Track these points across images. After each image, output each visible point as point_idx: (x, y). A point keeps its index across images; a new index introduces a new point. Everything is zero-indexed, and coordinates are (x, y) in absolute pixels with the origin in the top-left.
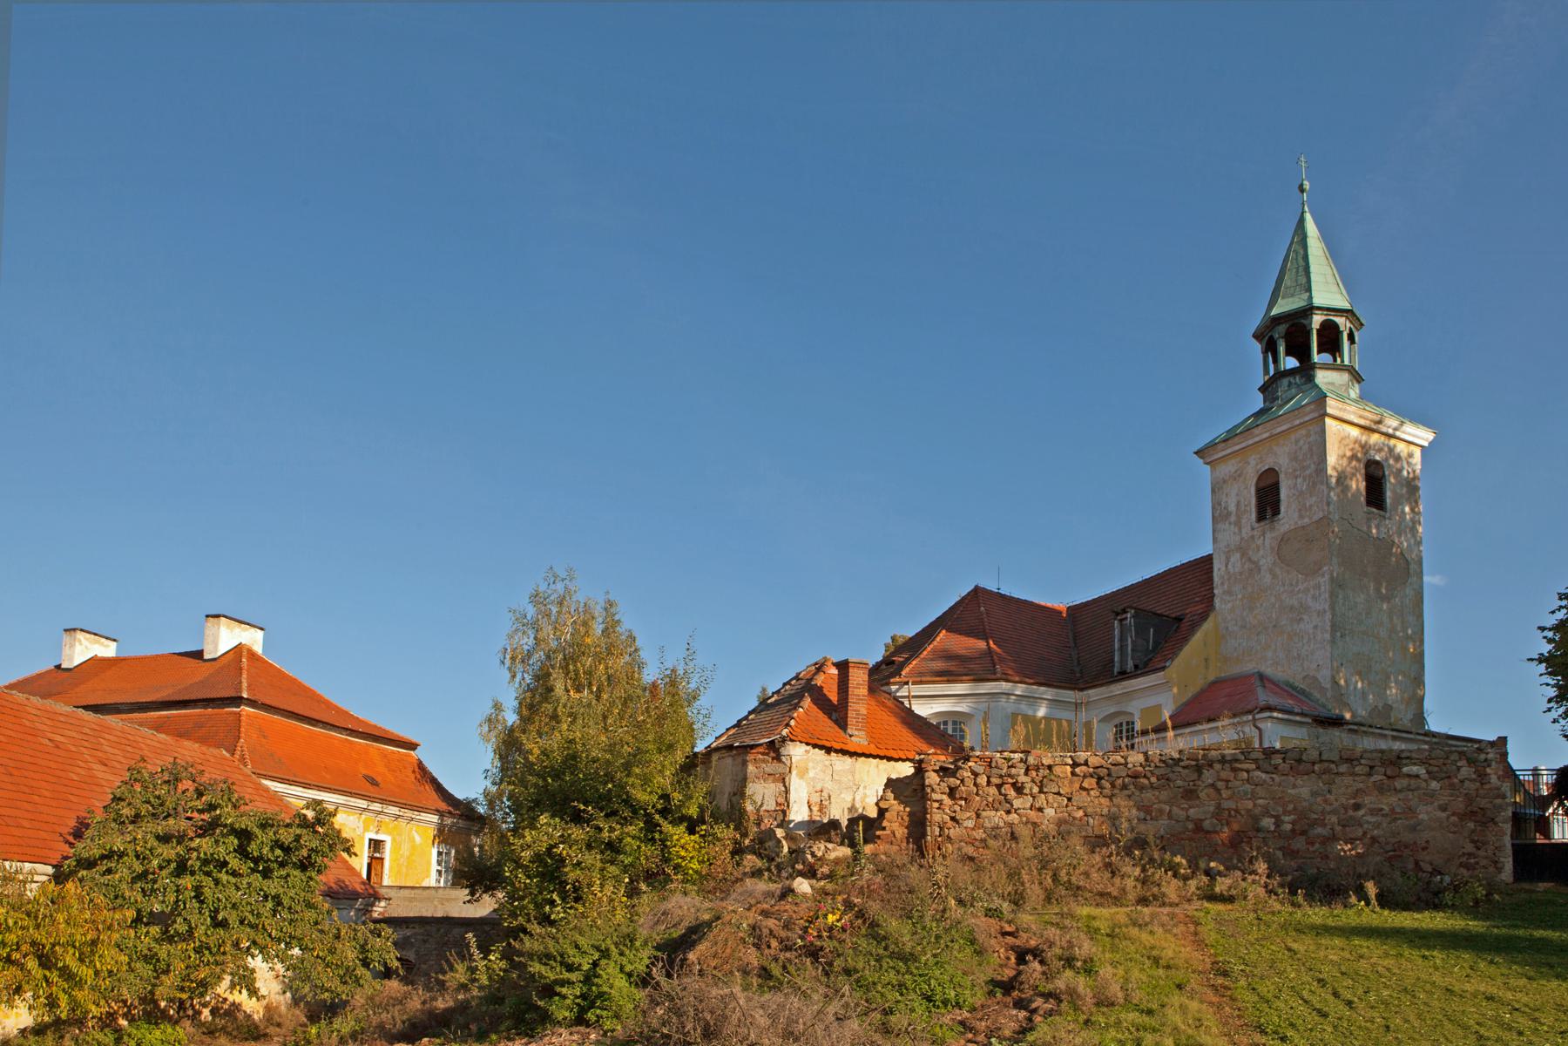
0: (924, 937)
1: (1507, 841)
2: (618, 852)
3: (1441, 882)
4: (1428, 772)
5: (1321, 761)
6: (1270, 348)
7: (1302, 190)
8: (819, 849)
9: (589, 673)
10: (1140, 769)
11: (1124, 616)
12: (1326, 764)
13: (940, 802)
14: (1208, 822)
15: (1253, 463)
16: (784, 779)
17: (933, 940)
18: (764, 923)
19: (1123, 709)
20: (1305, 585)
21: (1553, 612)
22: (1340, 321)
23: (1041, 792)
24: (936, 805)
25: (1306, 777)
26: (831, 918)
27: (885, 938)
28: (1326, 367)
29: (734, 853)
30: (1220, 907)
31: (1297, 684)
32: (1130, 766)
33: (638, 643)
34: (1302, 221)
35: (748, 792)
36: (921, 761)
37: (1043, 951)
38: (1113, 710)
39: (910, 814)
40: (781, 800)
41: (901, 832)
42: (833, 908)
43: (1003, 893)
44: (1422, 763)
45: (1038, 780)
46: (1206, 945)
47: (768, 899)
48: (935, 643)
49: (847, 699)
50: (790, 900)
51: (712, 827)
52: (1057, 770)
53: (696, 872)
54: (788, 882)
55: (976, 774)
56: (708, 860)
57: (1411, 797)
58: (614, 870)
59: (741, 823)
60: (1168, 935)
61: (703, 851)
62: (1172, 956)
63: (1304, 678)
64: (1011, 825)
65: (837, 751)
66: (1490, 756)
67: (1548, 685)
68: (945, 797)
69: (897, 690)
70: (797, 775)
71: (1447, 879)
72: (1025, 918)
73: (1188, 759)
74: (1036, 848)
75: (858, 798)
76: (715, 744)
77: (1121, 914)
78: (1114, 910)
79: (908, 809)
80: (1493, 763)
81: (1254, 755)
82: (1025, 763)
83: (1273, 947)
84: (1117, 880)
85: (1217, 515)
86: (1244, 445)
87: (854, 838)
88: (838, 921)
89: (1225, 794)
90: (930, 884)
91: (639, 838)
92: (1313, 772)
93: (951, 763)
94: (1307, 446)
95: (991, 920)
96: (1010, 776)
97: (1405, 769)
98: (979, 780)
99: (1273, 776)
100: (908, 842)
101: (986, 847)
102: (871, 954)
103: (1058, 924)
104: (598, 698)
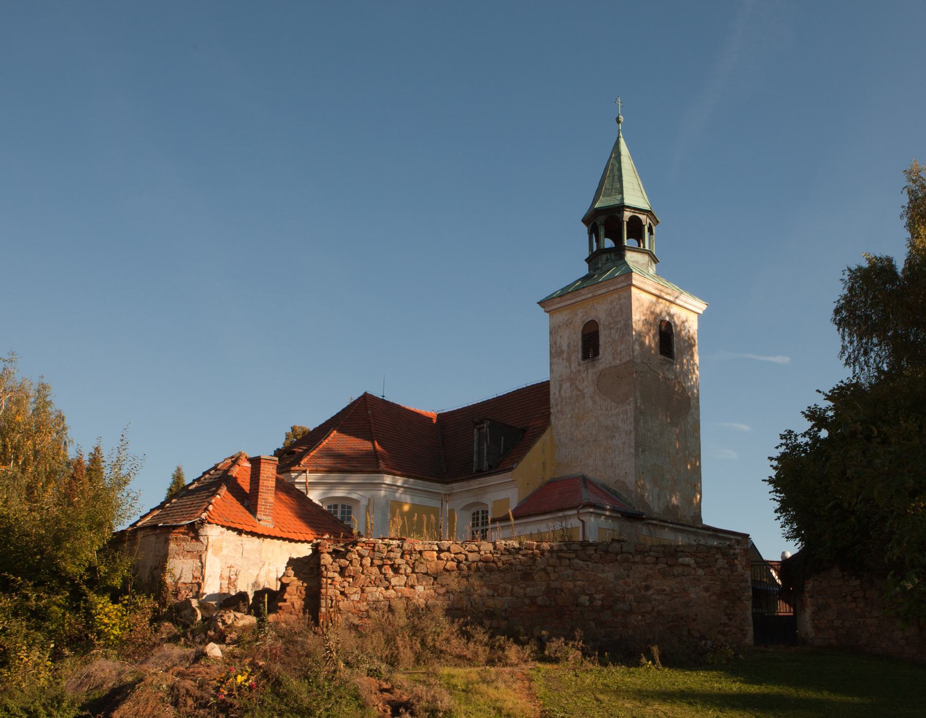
0: (319, 694)
1: (749, 612)
2: (44, 619)
3: (705, 645)
4: (696, 562)
5: (622, 553)
6: (593, 231)
7: (618, 122)
8: (229, 617)
9: (16, 448)
10: (490, 555)
11: (482, 426)
12: (626, 555)
13: (333, 579)
14: (540, 598)
15: (580, 315)
16: (200, 556)
17: (325, 697)
18: (182, 684)
19: (480, 501)
20: (616, 410)
21: (777, 448)
22: (643, 217)
23: (413, 572)
24: (329, 581)
25: (612, 564)
26: (240, 679)
27: (286, 695)
28: (632, 249)
29: (152, 621)
30: (548, 667)
31: (610, 486)
32: (482, 553)
33: (67, 422)
34: (617, 143)
35: (169, 566)
36: (317, 545)
37: (413, 704)
38: (471, 501)
39: (307, 589)
40: (197, 574)
41: (299, 603)
42: (242, 670)
43: (382, 656)
44: (692, 555)
45: (411, 562)
46: (537, 698)
47: (184, 662)
48: (330, 438)
49: (258, 489)
50: (203, 663)
51: (134, 597)
52: (427, 555)
53: (117, 637)
54: (201, 647)
55: (362, 557)
56: (129, 626)
57: (684, 581)
58: (40, 636)
59: (160, 594)
60: (509, 690)
61: (125, 619)
62: (511, 706)
63: (615, 482)
64: (388, 599)
65: (247, 533)
66: (737, 551)
67: (774, 499)
68: (336, 575)
69: (296, 477)
70: (212, 552)
71: (709, 643)
72: (400, 677)
73: (526, 549)
74: (408, 618)
75: (263, 573)
76: (140, 523)
77: (473, 673)
78: (468, 669)
79: (305, 585)
80: (739, 556)
81: (574, 547)
82: (401, 548)
83: (586, 699)
84: (471, 645)
85: (553, 352)
86: (573, 301)
87: (259, 608)
88: (246, 681)
89: (553, 576)
90: (323, 649)
91: (64, 607)
92: (616, 561)
93: (342, 547)
94: (618, 306)
95: (372, 679)
96: (389, 558)
97: (680, 560)
98: (364, 562)
99: (589, 563)
100: (304, 613)
101: (369, 617)
102: (275, 710)
103: (425, 681)
104: (23, 471)
